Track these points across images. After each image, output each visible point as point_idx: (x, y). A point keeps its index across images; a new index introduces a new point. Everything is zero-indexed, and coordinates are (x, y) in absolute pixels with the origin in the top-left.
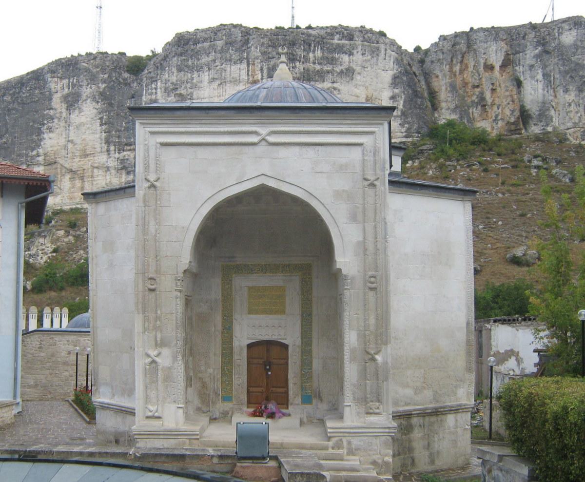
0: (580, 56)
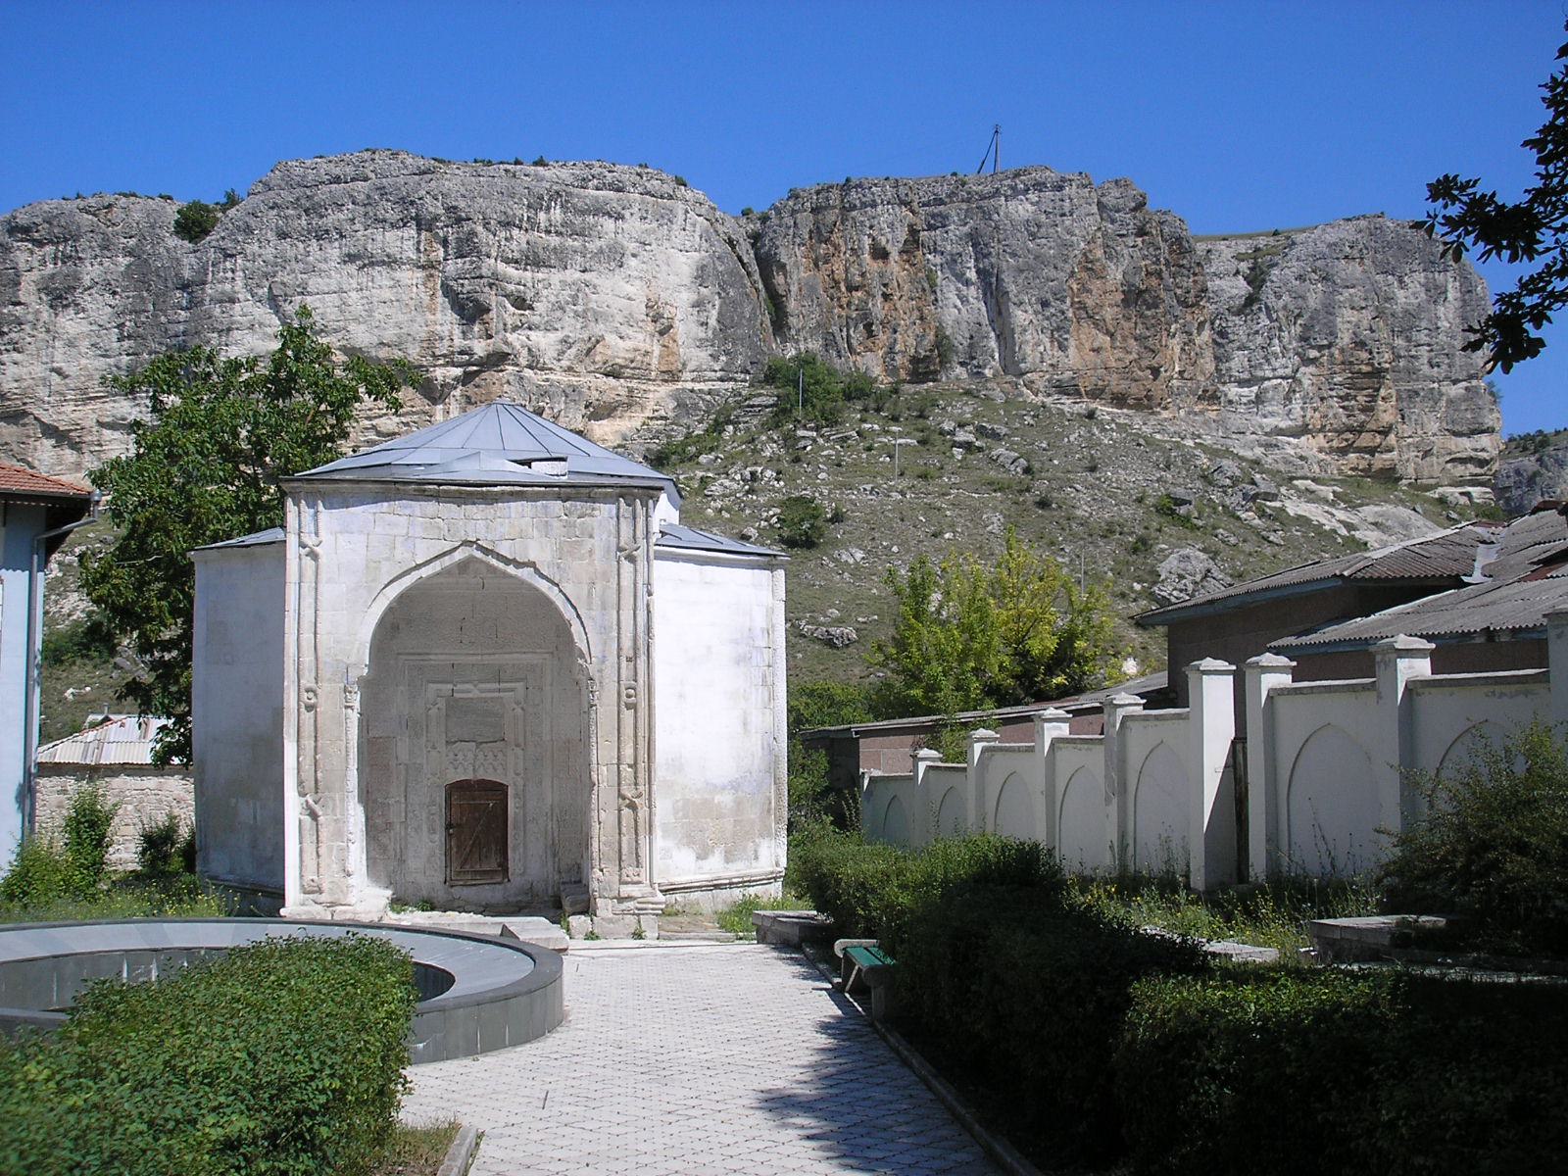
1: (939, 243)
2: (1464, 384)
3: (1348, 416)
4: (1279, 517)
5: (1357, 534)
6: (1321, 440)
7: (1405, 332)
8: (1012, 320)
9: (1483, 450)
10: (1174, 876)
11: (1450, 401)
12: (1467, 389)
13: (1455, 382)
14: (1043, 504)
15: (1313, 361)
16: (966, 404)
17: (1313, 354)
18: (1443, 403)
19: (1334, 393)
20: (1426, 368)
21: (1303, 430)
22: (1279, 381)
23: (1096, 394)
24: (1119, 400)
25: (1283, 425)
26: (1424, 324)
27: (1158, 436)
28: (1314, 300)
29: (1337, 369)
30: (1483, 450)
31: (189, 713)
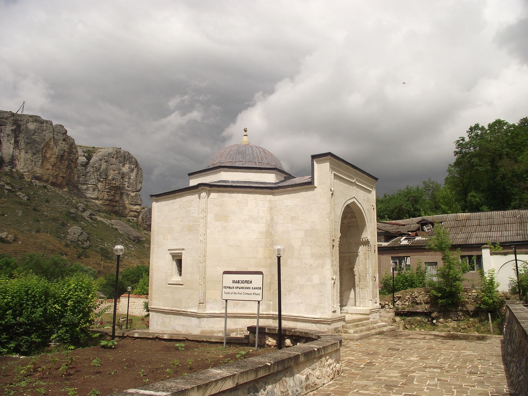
0: (36, 137)
1: (3, 130)
2: (135, 193)
3: (109, 197)
4: (95, 220)
5: (114, 226)
6: (101, 202)
7: (123, 178)
8: (4, 159)
9: (138, 209)
10: (435, 295)
11: (132, 196)
12: (135, 194)
13: (133, 192)
14: (35, 210)
15: (101, 181)
16: (7, 178)
17: (102, 180)
18: (130, 197)
19: (105, 190)
20: (127, 188)
21: (97, 199)
22: (92, 185)
23: (47, 181)
24: (53, 184)
25: (92, 197)
26: (127, 177)
27: (63, 195)
28: (104, 166)
29: (107, 185)
30: (138, 209)
31: (468, 135)
